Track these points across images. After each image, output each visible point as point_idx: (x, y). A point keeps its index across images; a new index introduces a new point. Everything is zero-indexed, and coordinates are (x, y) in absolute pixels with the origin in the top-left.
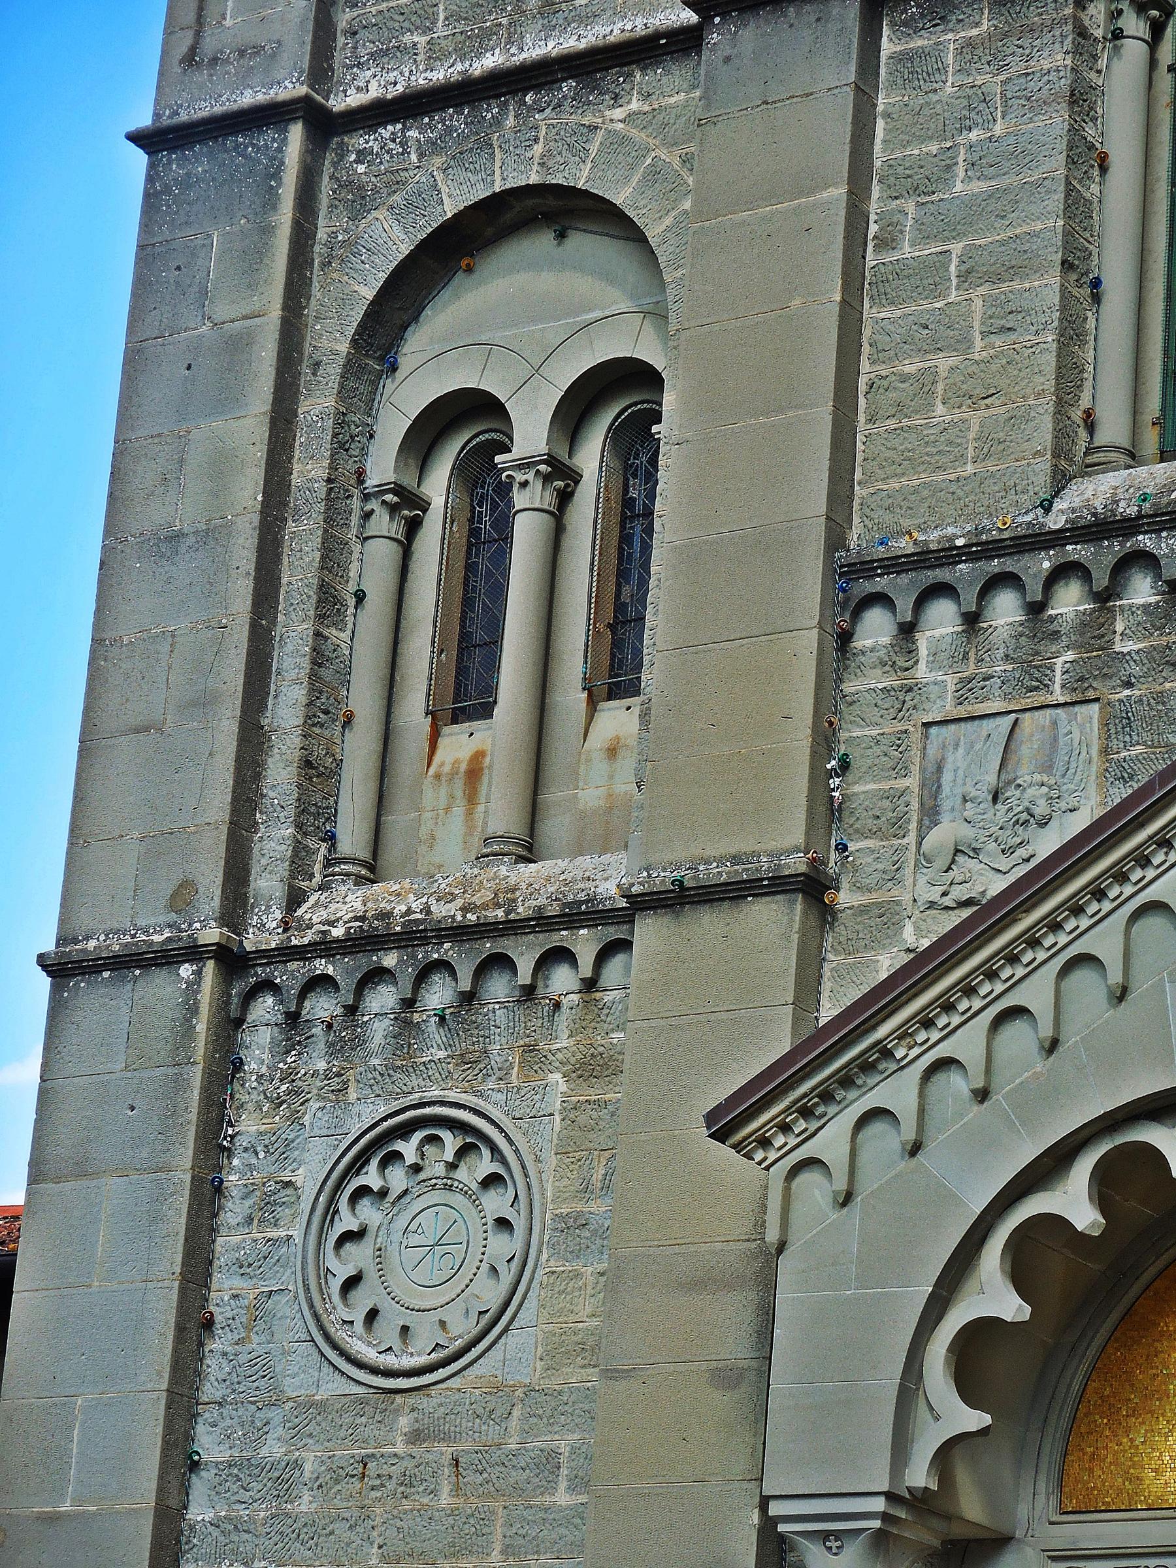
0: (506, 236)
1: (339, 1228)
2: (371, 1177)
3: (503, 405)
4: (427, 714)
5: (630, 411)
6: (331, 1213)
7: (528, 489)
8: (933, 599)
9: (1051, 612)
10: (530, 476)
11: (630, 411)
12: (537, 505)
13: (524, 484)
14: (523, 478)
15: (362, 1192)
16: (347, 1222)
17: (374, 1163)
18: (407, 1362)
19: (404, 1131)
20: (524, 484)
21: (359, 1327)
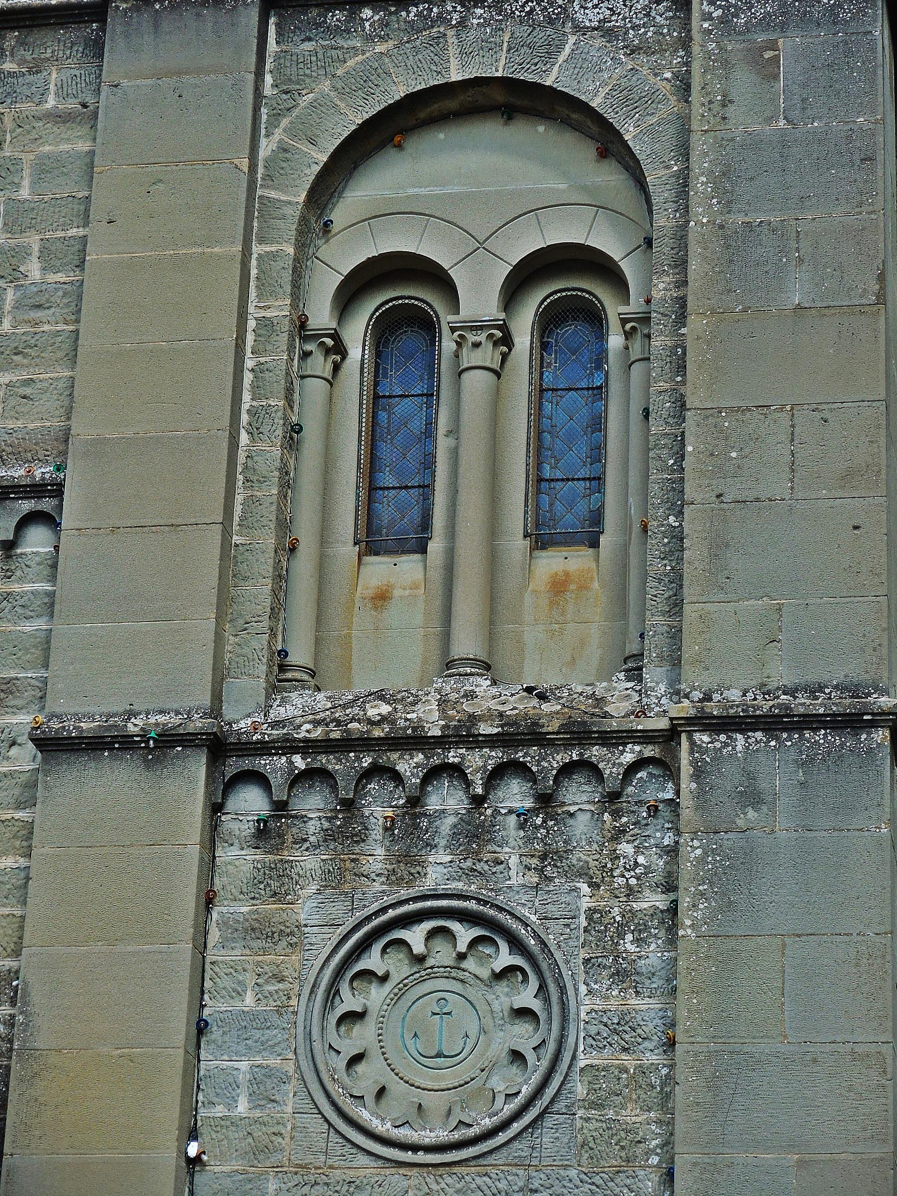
0: (530, 114)
1: (340, 1010)
2: (373, 961)
3: (515, 267)
4: (525, 537)
5: (391, 304)
6: (332, 993)
7: (480, 349)
8: (26, 527)
9: (19, 551)
10: (482, 337)
11: (391, 304)
12: (488, 364)
13: (477, 345)
14: (477, 339)
15: (367, 975)
16: (349, 1002)
17: (377, 948)
18: (428, 1137)
19: (408, 920)
20: (477, 345)
21: (370, 1099)
